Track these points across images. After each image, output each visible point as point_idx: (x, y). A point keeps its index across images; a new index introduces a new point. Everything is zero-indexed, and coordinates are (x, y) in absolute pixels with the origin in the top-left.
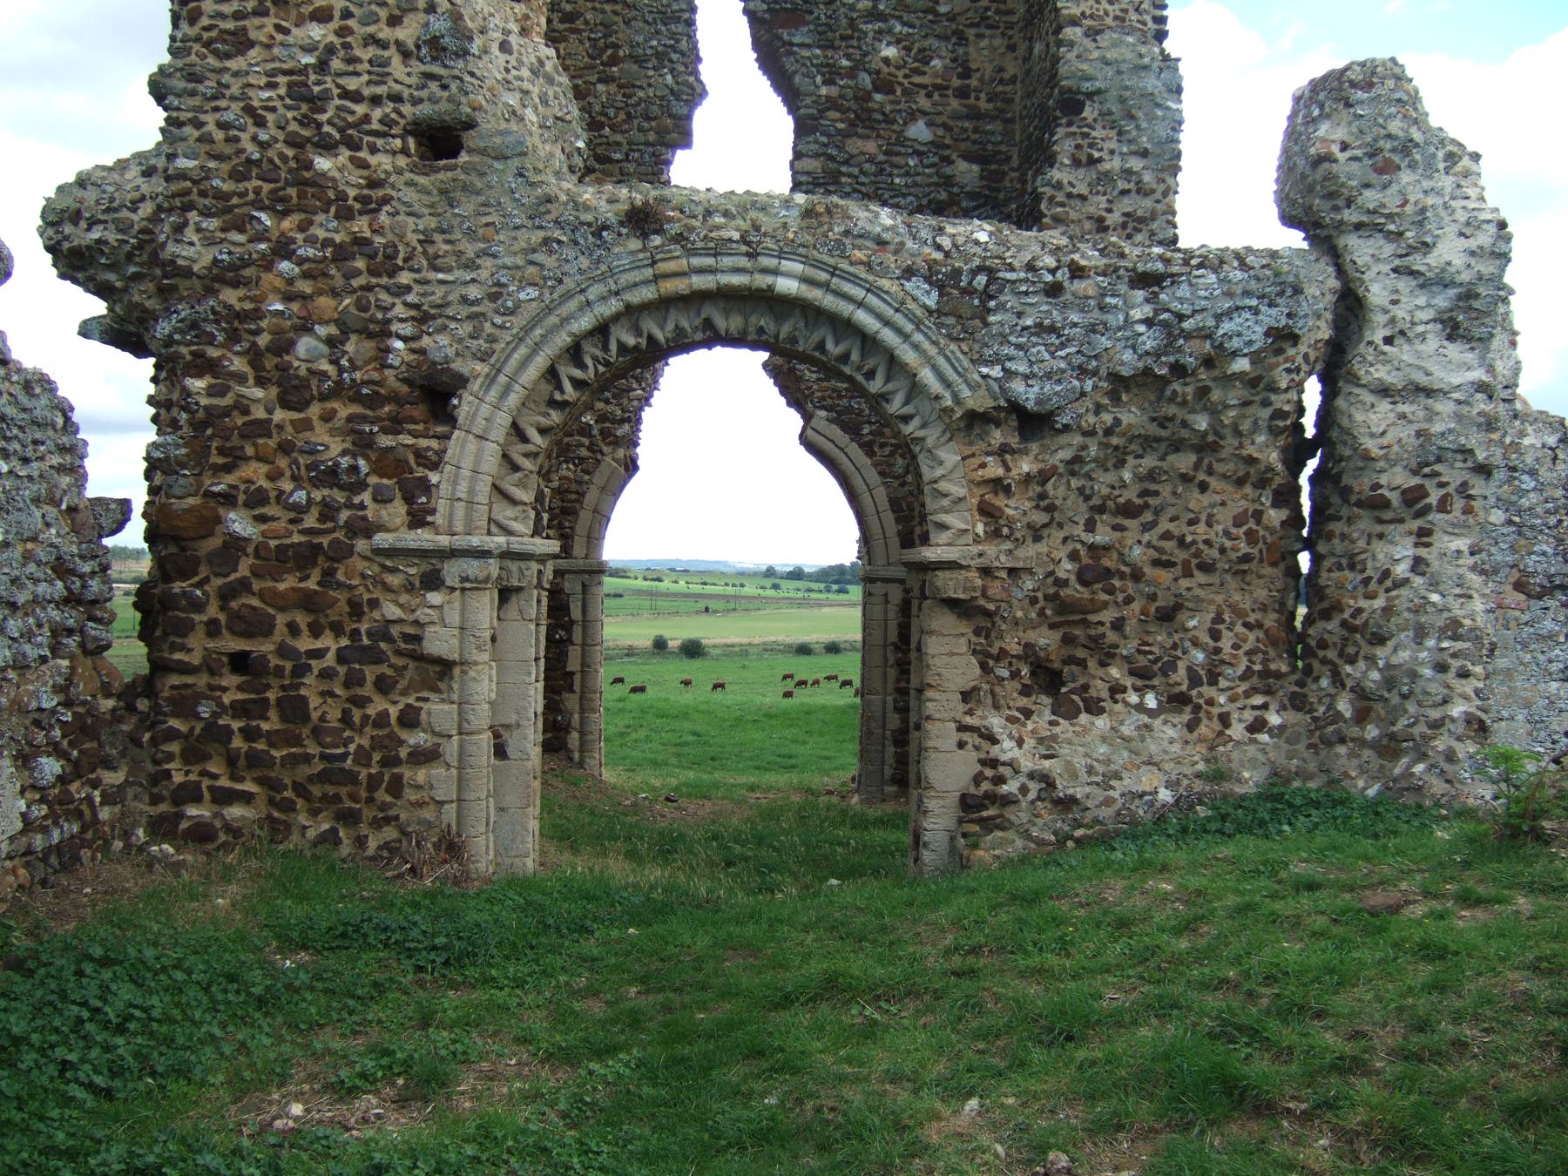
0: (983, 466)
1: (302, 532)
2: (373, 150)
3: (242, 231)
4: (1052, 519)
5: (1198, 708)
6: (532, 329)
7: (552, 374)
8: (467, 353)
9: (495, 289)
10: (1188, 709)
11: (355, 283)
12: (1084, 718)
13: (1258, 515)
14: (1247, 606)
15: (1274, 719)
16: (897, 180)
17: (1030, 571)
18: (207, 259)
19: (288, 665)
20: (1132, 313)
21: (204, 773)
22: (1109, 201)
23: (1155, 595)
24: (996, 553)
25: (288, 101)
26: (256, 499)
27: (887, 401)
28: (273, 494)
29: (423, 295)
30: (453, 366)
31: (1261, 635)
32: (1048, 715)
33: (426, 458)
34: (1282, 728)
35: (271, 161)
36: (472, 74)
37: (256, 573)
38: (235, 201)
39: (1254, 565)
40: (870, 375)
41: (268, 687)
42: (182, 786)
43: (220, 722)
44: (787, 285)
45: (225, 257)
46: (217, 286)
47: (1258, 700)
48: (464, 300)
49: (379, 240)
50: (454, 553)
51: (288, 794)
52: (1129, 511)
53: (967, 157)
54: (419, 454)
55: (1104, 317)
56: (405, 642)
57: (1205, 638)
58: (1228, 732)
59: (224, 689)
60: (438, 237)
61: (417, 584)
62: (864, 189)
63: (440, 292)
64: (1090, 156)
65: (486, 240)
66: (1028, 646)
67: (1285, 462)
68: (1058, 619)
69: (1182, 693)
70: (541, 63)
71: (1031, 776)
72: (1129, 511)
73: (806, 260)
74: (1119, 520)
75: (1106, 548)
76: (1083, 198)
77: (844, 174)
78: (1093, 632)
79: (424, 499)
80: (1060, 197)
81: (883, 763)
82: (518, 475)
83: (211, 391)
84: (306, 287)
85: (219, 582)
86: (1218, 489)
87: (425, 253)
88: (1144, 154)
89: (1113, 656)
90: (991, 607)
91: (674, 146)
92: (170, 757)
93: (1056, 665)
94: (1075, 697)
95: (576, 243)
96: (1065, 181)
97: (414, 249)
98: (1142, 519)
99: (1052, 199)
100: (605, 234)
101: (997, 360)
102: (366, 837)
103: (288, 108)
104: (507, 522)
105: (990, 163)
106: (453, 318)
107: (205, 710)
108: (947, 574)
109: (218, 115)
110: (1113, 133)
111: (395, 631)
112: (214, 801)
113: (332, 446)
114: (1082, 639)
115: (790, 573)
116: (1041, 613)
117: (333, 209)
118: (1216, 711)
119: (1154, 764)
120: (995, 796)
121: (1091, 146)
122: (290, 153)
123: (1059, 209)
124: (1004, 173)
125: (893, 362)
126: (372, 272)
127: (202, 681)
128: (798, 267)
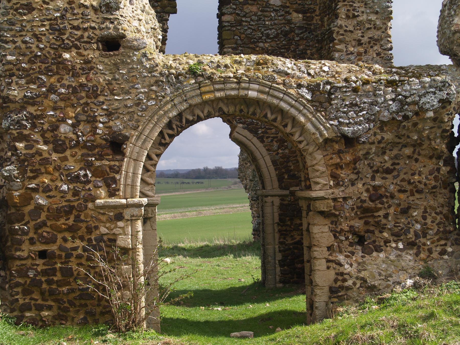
0: (332, 158)
1: (65, 201)
2: (85, 50)
3: (34, 83)
4: (359, 176)
5: (419, 247)
6: (153, 116)
7: (161, 133)
8: (128, 127)
9: (137, 102)
10: (415, 247)
11: (82, 102)
12: (375, 254)
13: (438, 170)
14: (436, 205)
15: (450, 249)
16: (267, 23)
17: (351, 198)
18: (21, 95)
19: (64, 254)
20: (387, 96)
21: (31, 299)
22: (362, 33)
23: (400, 203)
24: (339, 193)
25: (50, 31)
26: (47, 189)
27: (292, 135)
28: (54, 187)
29: (109, 105)
30: (122, 132)
31: (442, 217)
32: (361, 254)
33: (114, 169)
34: (453, 252)
35: (45, 55)
36: (122, 16)
37: (48, 218)
38: (31, 72)
39: (438, 190)
40: (285, 126)
41: (56, 263)
42: (23, 305)
43: (37, 278)
44: (252, 94)
45: (29, 94)
46: (25, 105)
47: (443, 242)
48: (126, 106)
49: (90, 84)
50: (128, 206)
51: (66, 305)
52: (388, 171)
53: (297, 11)
54: (111, 167)
55: (376, 99)
56: (109, 242)
57: (420, 219)
58: (431, 256)
59: (38, 265)
60: (114, 82)
61: (113, 219)
62: (253, 27)
63: (116, 104)
64: (354, 14)
65: (132, 82)
66: (351, 227)
67: (447, 148)
68: (362, 215)
69: (413, 242)
70: (144, 7)
71: (357, 278)
72: (388, 171)
73: (260, 84)
74: (384, 175)
75: (380, 187)
76: (351, 32)
77: (244, 21)
78: (376, 220)
79: (114, 186)
80: (342, 32)
81: (275, 274)
82: (149, 173)
83: (26, 147)
84: (62, 104)
85: (34, 223)
86: (422, 161)
87: (109, 88)
88: (377, 13)
89: (385, 228)
90: (337, 213)
91: (169, 13)
92: (17, 293)
93: (362, 233)
94: (370, 246)
95: (169, 81)
96: (343, 25)
97: (104, 87)
98: (393, 174)
99: (338, 32)
100: (180, 77)
101: (336, 118)
102: (98, 319)
103: (51, 34)
104: (146, 192)
105: (307, 13)
106: (121, 114)
107: (31, 274)
108: (320, 202)
109: (22, 38)
110: (362, 4)
111: (105, 238)
112: (36, 309)
113: (76, 166)
114: (372, 223)
115: (172, 174)
116: (356, 214)
117: (71, 73)
118: (426, 248)
119: (404, 270)
120: (343, 287)
121: (354, 10)
122: (52, 52)
123: (341, 37)
124: (313, 17)
125: (294, 119)
126: (88, 97)
127: (29, 262)
128: (256, 87)
